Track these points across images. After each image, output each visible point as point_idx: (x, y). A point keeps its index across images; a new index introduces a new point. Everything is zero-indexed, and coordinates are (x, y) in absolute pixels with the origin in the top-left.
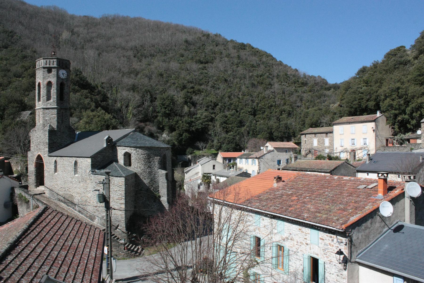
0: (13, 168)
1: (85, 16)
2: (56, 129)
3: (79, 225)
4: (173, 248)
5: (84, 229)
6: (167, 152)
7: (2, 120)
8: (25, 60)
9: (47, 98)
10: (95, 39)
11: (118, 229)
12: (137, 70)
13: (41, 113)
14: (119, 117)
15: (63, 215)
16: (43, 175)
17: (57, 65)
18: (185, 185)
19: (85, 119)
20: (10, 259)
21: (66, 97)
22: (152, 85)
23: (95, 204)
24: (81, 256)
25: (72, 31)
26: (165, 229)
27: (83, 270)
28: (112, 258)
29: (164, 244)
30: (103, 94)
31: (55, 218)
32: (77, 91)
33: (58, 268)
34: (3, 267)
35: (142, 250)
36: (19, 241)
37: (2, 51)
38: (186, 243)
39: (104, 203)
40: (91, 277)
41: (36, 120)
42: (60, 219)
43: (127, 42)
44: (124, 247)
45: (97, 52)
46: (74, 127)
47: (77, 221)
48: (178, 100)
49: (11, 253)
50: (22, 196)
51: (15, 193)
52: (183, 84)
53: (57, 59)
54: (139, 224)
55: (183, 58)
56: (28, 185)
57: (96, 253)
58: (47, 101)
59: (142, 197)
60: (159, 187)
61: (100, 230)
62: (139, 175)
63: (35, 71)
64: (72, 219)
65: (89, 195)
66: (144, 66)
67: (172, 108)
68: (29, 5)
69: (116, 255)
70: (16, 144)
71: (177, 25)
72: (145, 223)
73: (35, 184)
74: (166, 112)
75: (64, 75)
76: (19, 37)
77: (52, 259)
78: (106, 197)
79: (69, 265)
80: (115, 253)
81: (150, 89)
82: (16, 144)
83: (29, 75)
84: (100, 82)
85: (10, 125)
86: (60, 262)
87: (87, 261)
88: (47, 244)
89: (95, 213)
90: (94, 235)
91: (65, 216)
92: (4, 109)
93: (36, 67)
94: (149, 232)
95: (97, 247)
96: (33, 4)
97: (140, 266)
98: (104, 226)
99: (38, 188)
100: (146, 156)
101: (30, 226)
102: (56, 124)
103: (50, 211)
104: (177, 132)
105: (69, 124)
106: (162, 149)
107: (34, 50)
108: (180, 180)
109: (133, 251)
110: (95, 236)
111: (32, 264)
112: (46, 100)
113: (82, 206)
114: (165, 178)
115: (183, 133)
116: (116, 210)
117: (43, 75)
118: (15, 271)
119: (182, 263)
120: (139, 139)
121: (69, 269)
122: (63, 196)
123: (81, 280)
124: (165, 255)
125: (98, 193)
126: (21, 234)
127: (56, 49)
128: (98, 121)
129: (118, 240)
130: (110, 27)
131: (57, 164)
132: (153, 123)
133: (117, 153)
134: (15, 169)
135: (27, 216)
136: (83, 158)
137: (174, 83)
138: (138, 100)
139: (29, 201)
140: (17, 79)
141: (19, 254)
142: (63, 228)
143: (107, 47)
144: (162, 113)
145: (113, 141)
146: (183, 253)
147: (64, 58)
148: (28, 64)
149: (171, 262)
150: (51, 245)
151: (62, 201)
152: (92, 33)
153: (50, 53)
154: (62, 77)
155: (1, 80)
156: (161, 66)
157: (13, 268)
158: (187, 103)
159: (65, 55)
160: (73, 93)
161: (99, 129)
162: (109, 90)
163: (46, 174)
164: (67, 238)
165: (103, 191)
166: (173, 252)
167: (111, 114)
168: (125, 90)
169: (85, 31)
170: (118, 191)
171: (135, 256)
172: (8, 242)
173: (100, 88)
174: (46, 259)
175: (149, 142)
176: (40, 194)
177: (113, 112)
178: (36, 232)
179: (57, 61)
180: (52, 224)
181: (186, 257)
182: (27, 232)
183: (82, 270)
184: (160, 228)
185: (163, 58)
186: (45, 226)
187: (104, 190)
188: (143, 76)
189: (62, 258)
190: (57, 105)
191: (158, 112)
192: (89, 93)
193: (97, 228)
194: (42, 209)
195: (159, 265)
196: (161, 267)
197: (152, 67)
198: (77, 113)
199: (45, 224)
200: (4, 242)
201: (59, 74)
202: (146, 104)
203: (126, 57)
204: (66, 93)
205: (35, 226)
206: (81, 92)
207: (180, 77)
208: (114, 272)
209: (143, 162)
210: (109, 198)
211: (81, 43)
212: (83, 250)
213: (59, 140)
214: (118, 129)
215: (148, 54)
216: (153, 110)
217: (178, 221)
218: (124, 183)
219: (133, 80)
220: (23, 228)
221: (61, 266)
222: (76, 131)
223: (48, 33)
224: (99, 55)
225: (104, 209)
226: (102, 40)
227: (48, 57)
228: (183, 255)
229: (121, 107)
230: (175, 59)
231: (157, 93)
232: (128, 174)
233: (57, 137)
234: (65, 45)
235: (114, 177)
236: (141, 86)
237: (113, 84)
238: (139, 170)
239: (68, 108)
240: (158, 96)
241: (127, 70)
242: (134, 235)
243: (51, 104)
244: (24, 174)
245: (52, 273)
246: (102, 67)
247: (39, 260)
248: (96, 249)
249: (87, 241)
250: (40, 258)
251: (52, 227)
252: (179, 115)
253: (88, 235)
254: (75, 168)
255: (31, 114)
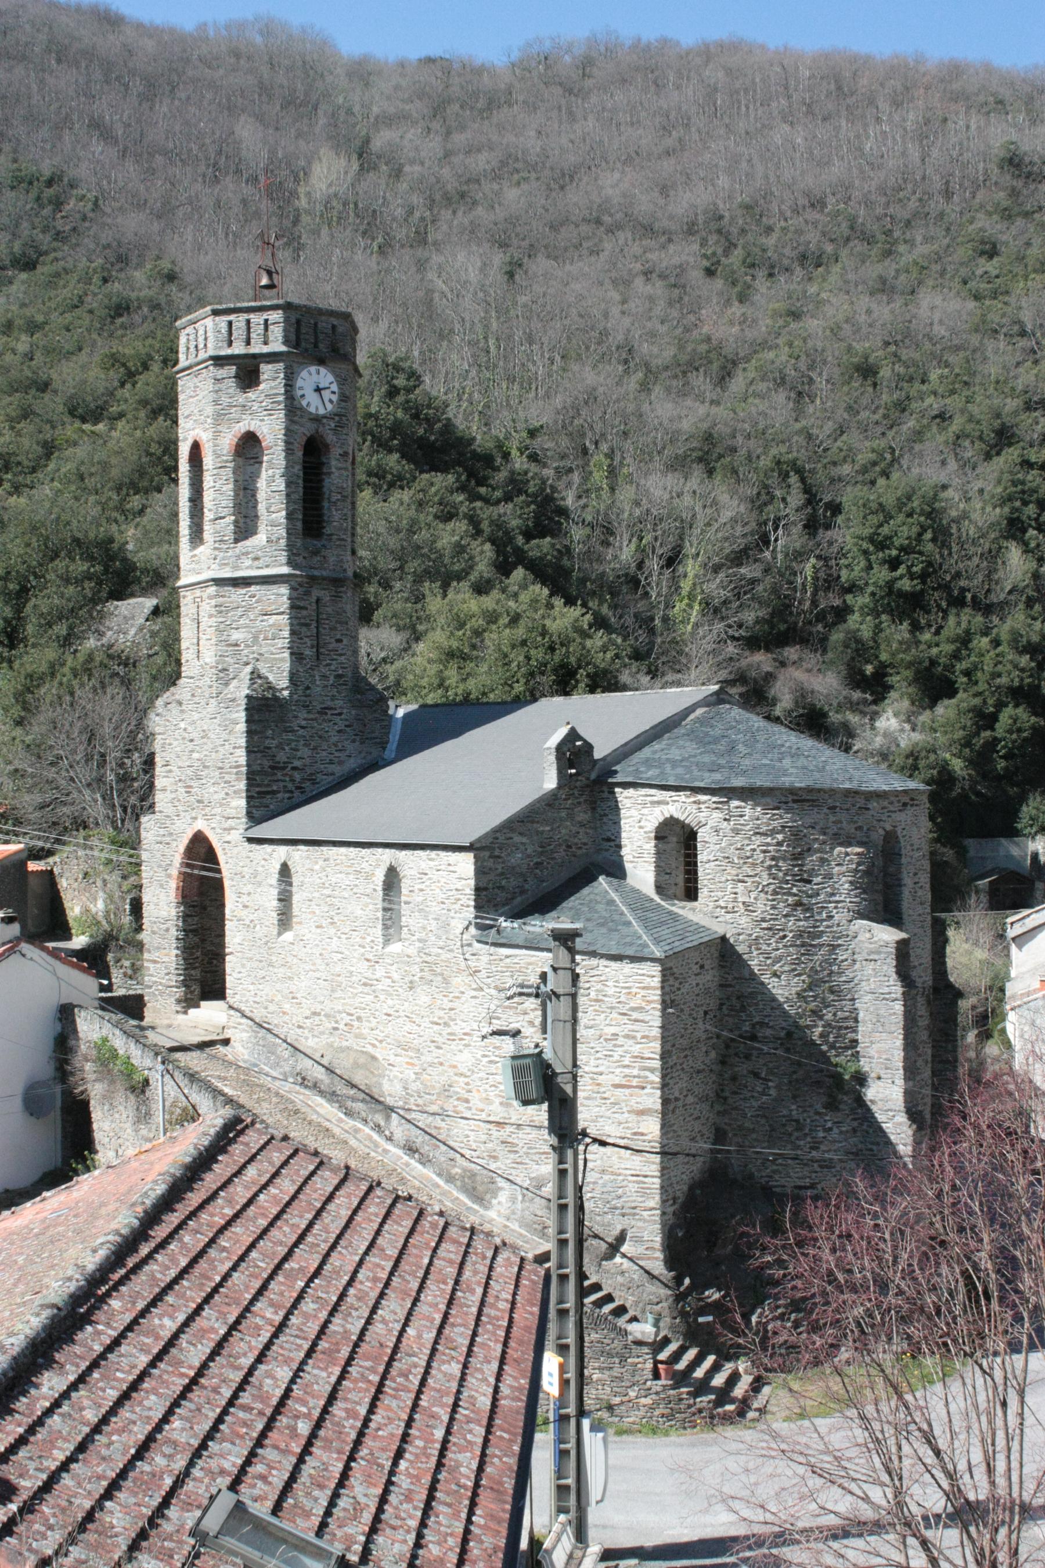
0: (67, 905)
1: (430, 61)
2: (286, 693)
3: (408, 1223)
4: (938, 1387)
5: (435, 1250)
6: (903, 818)
7: (12, 646)
8: (123, 327)
9: (236, 522)
10: (488, 187)
11: (624, 1256)
12: (728, 350)
13: (207, 607)
14: (629, 620)
15: (321, 1163)
16: (222, 945)
17: (286, 342)
18: (1012, 1016)
19: (438, 637)
20: (51, 1389)
21: (336, 515)
22: (815, 431)
23: (497, 1112)
24: (417, 1398)
25: (362, 152)
26: (890, 1274)
27: (426, 1480)
28: (586, 1423)
29: (887, 1360)
30: (535, 495)
31: (278, 1181)
32: (398, 482)
33: (294, 1460)
34: (13, 1428)
35: (757, 1385)
36: (94, 1295)
37: (11, 283)
38: (1018, 1359)
39: (545, 1106)
40: (469, 1521)
41: (184, 645)
42: (307, 1189)
43: (664, 190)
44: (656, 1363)
45: (498, 259)
46: (383, 678)
47: (397, 1198)
48: (965, 515)
49: (57, 1356)
50: (114, 1054)
51: (78, 1039)
52: (998, 416)
53: (287, 307)
54: (743, 1234)
55: (992, 266)
56: (140, 997)
57: (496, 1390)
58: (237, 541)
59: (756, 1075)
60: (856, 1021)
61: (522, 1259)
62: (740, 949)
63: (175, 384)
64: (370, 1189)
65: (465, 1059)
66: (765, 324)
67: (930, 564)
68: (139, 26)
69: (610, 1408)
70: (85, 773)
71: (955, 70)
72: (775, 1228)
73: (180, 992)
74: (899, 584)
75: (326, 394)
76: (90, 205)
77: (258, 1405)
78: (555, 1074)
79: (348, 1448)
80: (605, 1393)
81: (803, 455)
82: (85, 773)
83: (144, 403)
84: (520, 426)
85: (53, 675)
86: (304, 1428)
87: (448, 1432)
88: (238, 1322)
89: (495, 1158)
90: (487, 1285)
91: (334, 1170)
92: (23, 592)
93: (176, 362)
94: (798, 1283)
95: (504, 1353)
96: (158, 21)
97: (743, 1477)
98: (543, 1233)
99: (192, 1012)
100: (779, 844)
101: (152, 1217)
102: (287, 666)
103: (253, 1139)
104: (964, 699)
105: (356, 667)
106: (874, 805)
107: (165, 265)
108: (984, 983)
109: (702, 1387)
110: (491, 1292)
111: (158, 1428)
112: (230, 537)
113: (423, 1120)
114: (892, 971)
115: (1000, 705)
116: (609, 1149)
117: (216, 402)
118: (71, 1459)
119: (993, 1483)
120: (741, 747)
121: (347, 1468)
122: (325, 1062)
123: (413, 1535)
124: (889, 1431)
125: (512, 1048)
126: (108, 1258)
127: (280, 254)
128: (513, 647)
129: (621, 1322)
130: (570, 113)
131: (291, 884)
132: (825, 651)
133: (617, 823)
134: (77, 910)
135: (134, 1164)
136: (433, 854)
137: (942, 417)
138: (734, 520)
139: (146, 1082)
140: (85, 427)
141: (95, 1365)
142: (321, 1237)
143: (554, 227)
144: (873, 594)
145: (597, 755)
146: (999, 1422)
147: (322, 305)
148: (138, 344)
149: (927, 1476)
150: (258, 1328)
151: (315, 1086)
152: (468, 152)
153: (250, 277)
154: (312, 410)
155: (7, 438)
156: (862, 318)
157: (66, 1440)
158: (1024, 531)
159: (329, 288)
160: (376, 493)
161: (519, 688)
162: (570, 470)
163: (234, 937)
164: (342, 1296)
165: (538, 1037)
166: (938, 1413)
167: (584, 605)
168: (657, 463)
169: (433, 146)
170: (621, 1041)
171: (714, 1420)
172: (39, 1300)
173: (519, 462)
174: (231, 1403)
175: (802, 762)
176: (203, 1046)
177: (593, 593)
178: (178, 1254)
179: (286, 320)
180: (264, 1215)
181: (1015, 1446)
182: (137, 1251)
183: (418, 1478)
184: (864, 1268)
185: (873, 270)
186: (229, 1223)
187: (545, 1032)
188: (762, 380)
189: (312, 1402)
190: (289, 563)
191: (852, 588)
192: (462, 488)
193: (504, 1244)
194: (212, 1131)
195: (853, 1487)
196: (866, 1499)
197: (813, 324)
198: (396, 602)
199: (229, 1212)
200: (23, 1294)
201: (300, 393)
202: (783, 541)
203: (662, 277)
204: (335, 497)
205: (176, 1222)
206: (416, 486)
207: (978, 379)
208: (593, 1501)
209: (765, 875)
210: (575, 1077)
211: (410, 212)
212: (428, 1366)
213: (305, 752)
214: (624, 688)
215: (787, 251)
216: (822, 575)
217: (973, 1228)
218: (656, 995)
219: (702, 410)
220: (114, 1225)
221: (307, 1450)
222: (391, 704)
223: (238, 171)
224: (511, 275)
225: (545, 1140)
226: (525, 186)
227: (239, 299)
228: (1000, 1435)
229: (640, 565)
230: (943, 273)
231: (840, 480)
232: (679, 946)
233: (290, 736)
234: (325, 231)
235: (603, 962)
236: (748, 437)
237: (589, 434)
238: (743, 920)
239: (350, 573)
240: (850, 496)
241: (669, 353)
242: (713, 1295)
243: (256, 559)
244: (121, 937)
245: (260, 1484)
246: (530, 340)
247: (192, 1406)
248: (495, 1365)
249: (446, 1316)
250: (196, 1395)
251: (265, 1231)
252: (976, 604)
253: (457, 1282)
254: (385, 909)
255: (156, 612)
